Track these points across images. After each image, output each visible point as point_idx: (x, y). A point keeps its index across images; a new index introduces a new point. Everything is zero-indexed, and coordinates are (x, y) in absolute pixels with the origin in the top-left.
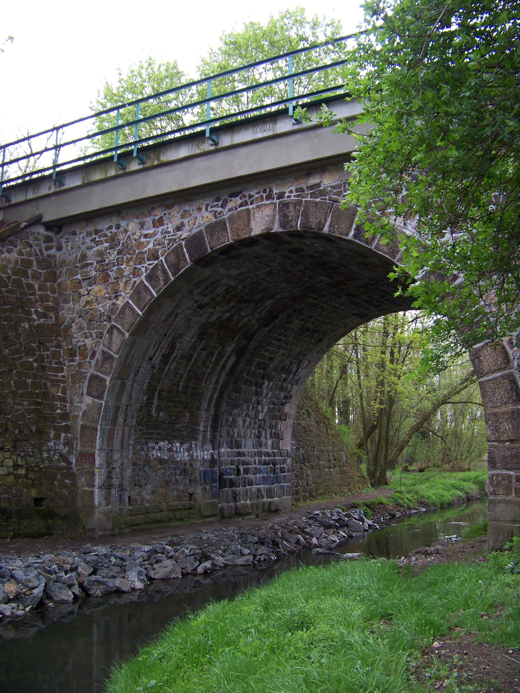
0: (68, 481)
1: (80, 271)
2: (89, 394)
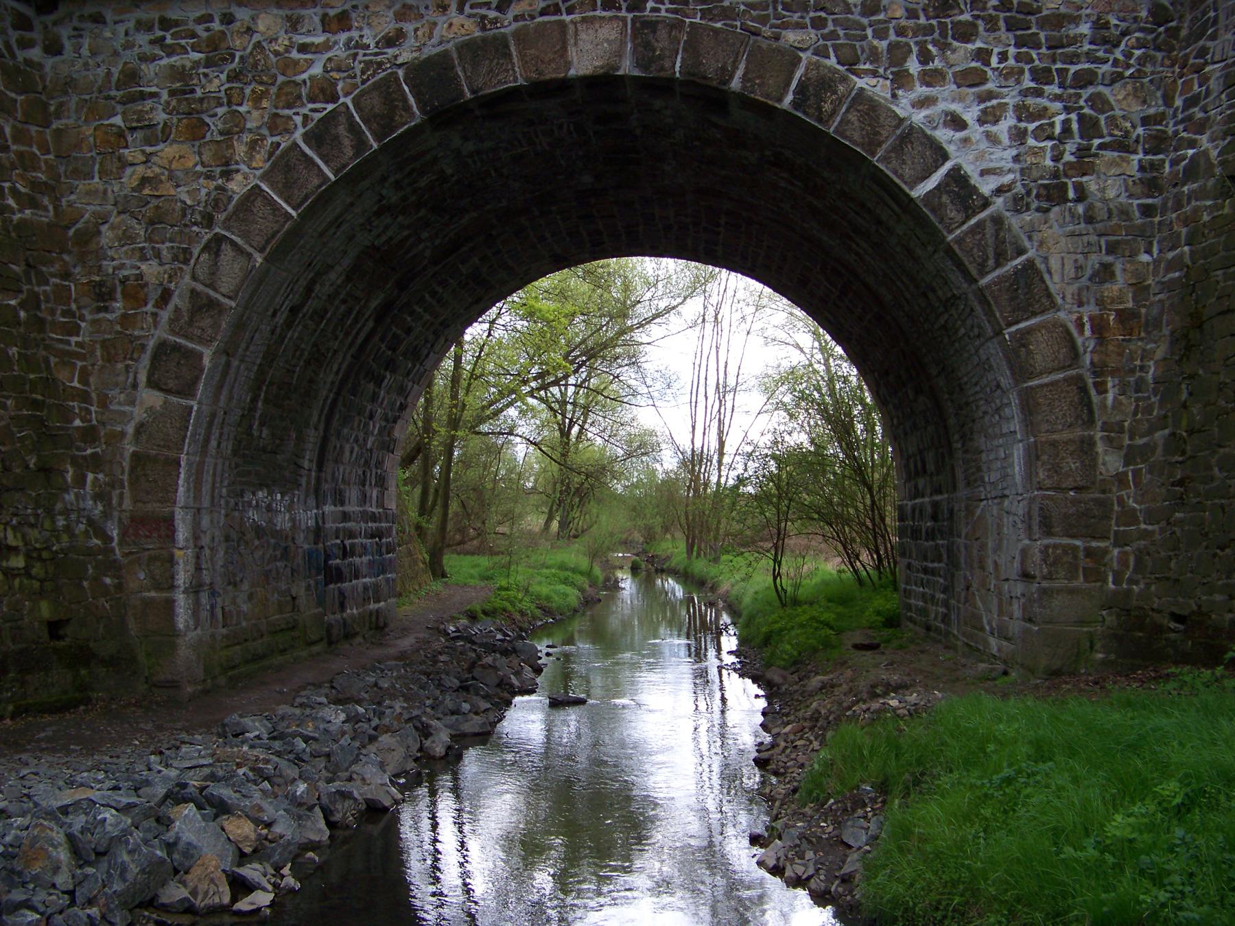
0: (108, 580)
1: (119, 108)
2: (153, 384)
